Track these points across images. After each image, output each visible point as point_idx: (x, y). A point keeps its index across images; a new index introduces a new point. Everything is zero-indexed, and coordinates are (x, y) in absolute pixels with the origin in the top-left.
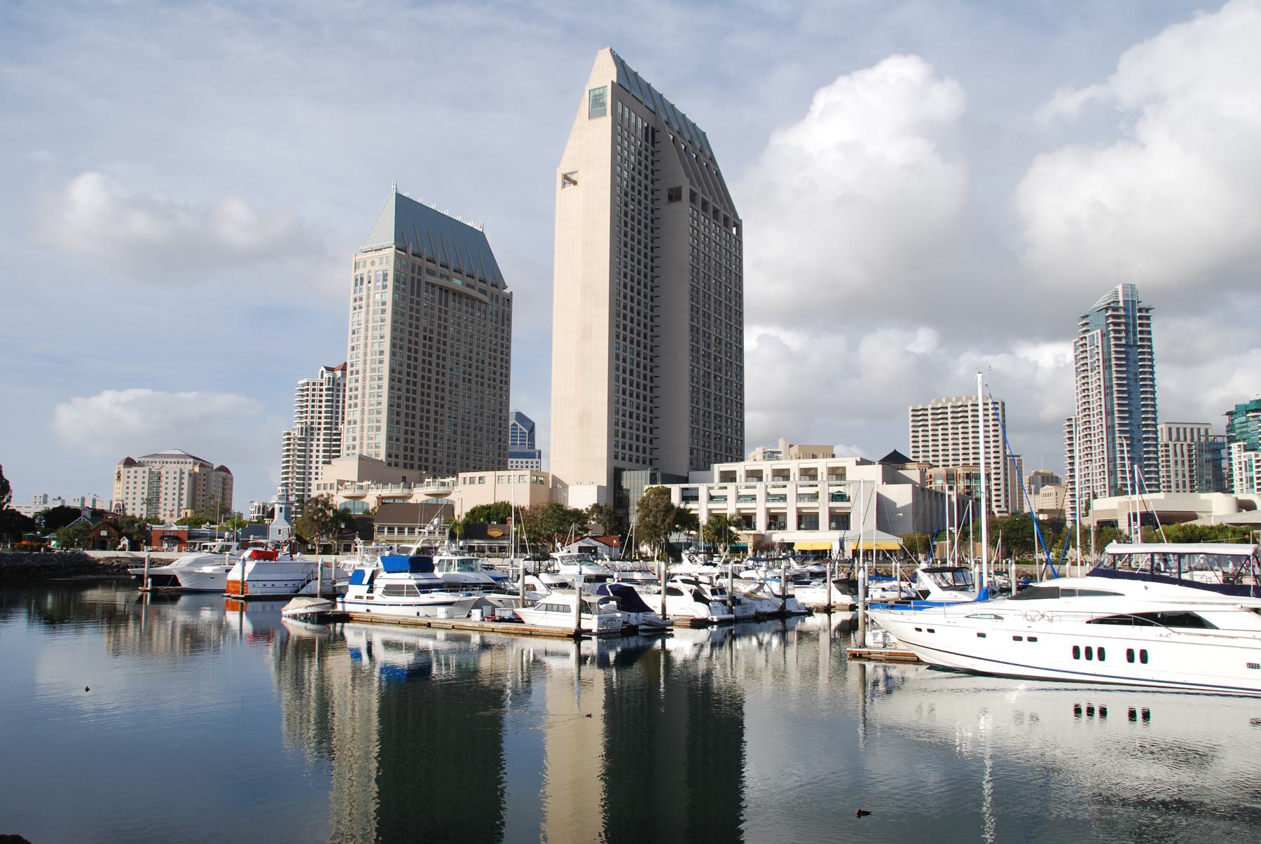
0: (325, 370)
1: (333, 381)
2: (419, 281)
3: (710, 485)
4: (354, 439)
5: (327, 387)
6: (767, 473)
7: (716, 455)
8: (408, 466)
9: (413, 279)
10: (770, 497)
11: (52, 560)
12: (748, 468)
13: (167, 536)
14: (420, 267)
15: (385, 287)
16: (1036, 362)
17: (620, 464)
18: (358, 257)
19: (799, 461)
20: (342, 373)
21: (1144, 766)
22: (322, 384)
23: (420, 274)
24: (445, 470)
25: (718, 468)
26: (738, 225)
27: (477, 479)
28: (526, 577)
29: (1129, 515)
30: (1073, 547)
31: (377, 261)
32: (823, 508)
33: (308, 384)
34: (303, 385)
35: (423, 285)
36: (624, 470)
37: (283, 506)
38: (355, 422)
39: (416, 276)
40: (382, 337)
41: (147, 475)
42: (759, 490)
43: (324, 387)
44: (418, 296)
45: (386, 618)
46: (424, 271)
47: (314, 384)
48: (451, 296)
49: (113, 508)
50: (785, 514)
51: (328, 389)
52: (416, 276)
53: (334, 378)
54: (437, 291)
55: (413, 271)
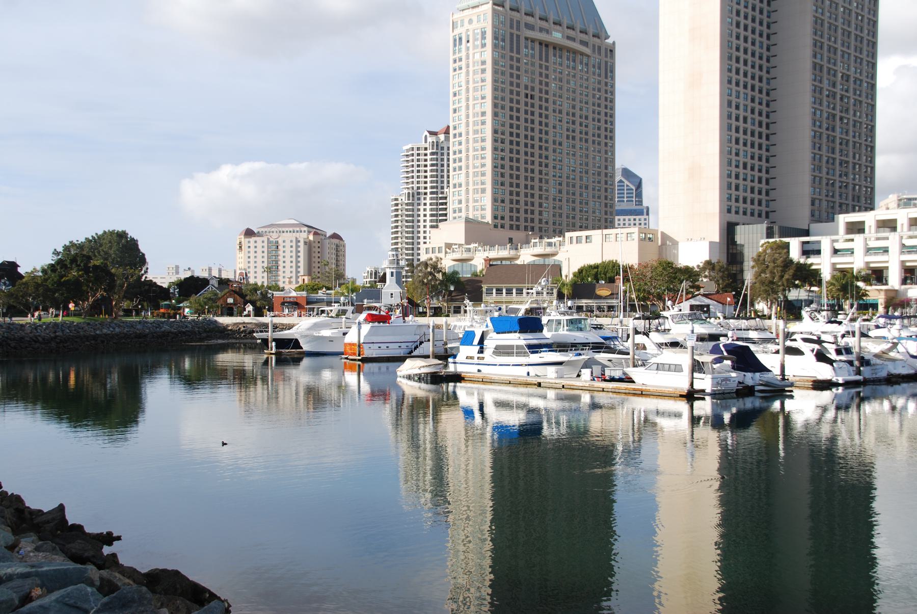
0: (428, 135)
1: (437, 145)
2: (518, 37)
4: (460, 202)
5: (431, 151)
7: (841, 205)
9: (512, 35)
13: (287, 302)
14: (518, 22)
15: (483, 46)
18: (455, 16)
20: (445, 137)
22: (426, 149)
23: (518, 29)
27: (584, 238)
31: (475, 19)
33: (413, 149)
34: (408, 150)
35: (522, 41)
36: (737, 224)
37: (394, 271)
38: (460, 185)
39: (515, 31)
40: (483, 98)
43: (428, 152)
46: (522, 25)
47: (418, 149)
48: (551, 51)
51: (432, 154)
52: (515, 31)
53: (437, 142)
54: (537, 46)
55: (511, 27)
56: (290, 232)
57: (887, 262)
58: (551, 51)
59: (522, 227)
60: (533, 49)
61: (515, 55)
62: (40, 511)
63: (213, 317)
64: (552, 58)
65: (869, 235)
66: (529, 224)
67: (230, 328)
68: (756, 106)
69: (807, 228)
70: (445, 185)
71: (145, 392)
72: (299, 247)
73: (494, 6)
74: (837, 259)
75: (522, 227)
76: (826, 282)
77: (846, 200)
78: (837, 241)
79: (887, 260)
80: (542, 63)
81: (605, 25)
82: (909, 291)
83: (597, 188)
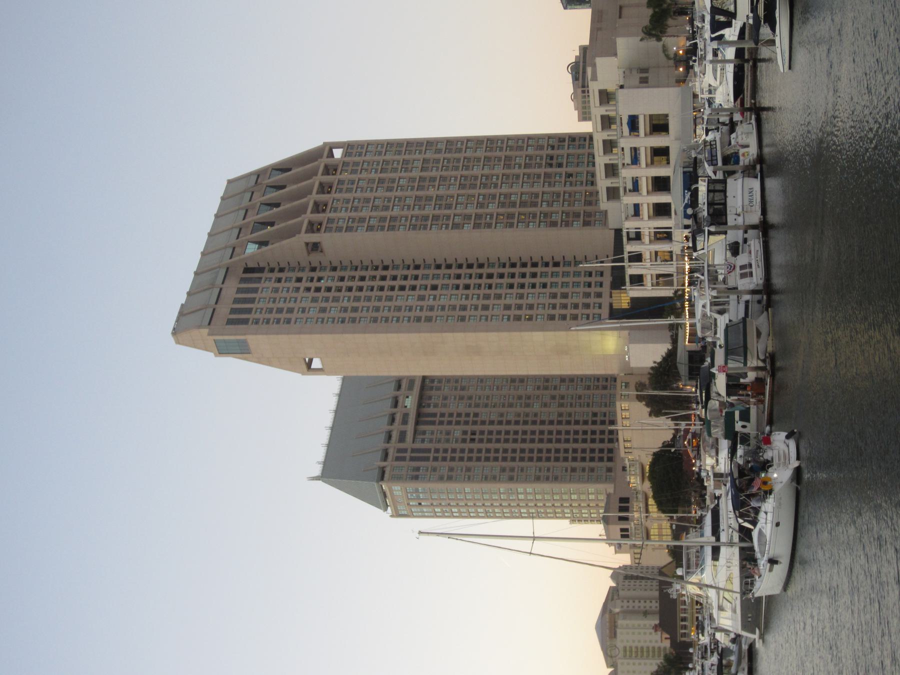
2: (413, 451)
3: (620, 166)
7: (589, 203)
8: (610, 455)
9: (412, 459)
10: (635, 160)
11: (700, 628)
12: (598, 103)
14: (400, 451)
17: (605, 312)
23: (405, 450)
24: (590, 188)
25: (604, 204)
28: (710, 237)
30: (698, 504)
32: (646, 142)
35: (418, 445)
36: (611, 305)
39: (408, 455)
41: (626, 661)
42: (627, 143)
44: (429, 451)
45: (758, 73)
48: (426, 410)
49: (648, 593)
50: (651, 116)
52: (408, 455)
54: (422, 428)
56: (628, 672)
57: (646, 148)
58: (426, 410)
60: (424, 433)
61: (431, 455)
63: (687, 256)
64: (431, 410)
65: (621, 183)
69: (613, 231)
70: (570, 464)
72: (639, 625)
74: (644, 190)
76: (682, 567)
78: (625, 188)
79: (646, 205)
80: (437, 421)
82: (677, 253)
83: (548, 161)
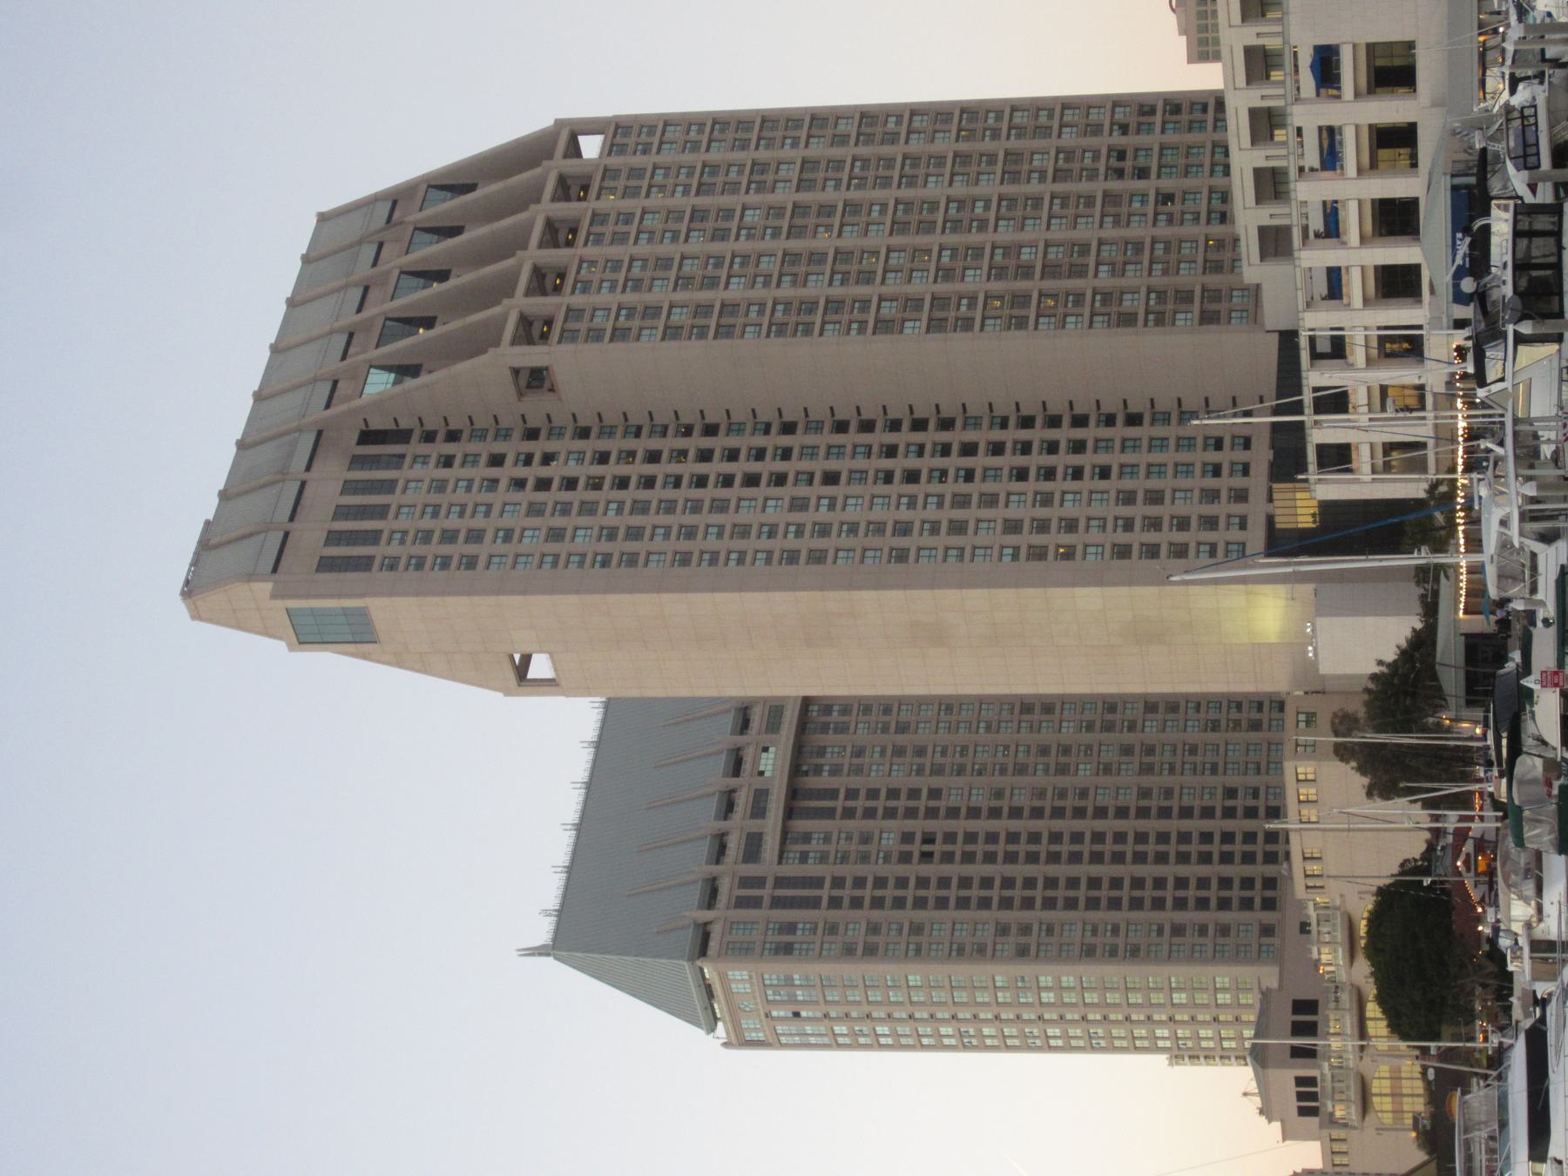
2: (780, 882)
3: (1293, 173)
6: (1266, 215)
7: (1213, 267)
8: (1269, 894)
9: (777, 903)
10: (1331, 158)
14: (746, 882)
16: (1270, 1122)
17: (1256, 537)
19: (1221, 27)
21: (1519, 911)
23: (759, 882)
24: (1217, 229)
25: (1253, 269)
26: (569, 134)
29: (1341, 329)
35: (792, 869)
36: (1270, 520)
39: (766, 893)
42: (1310, 115)
44: (817, 882)
46: (751, 870)
48: (812, 782)
50: (1371, 48)
52: (766, 893)
54: (801, 825)
55: (755, 903)
58: (812, 782)
59: (1269, 870)
60: (807, 838)
61: (825, 893)
62: (207, 523)
64: (824, 781)
66: (1257, 894)
67: (1528, 707)
68: (1036, 460)
71: (1533, 713)
73: (710, 952)
75: (1269, 870)
77: (1204, 147)
81: (450, 682)
